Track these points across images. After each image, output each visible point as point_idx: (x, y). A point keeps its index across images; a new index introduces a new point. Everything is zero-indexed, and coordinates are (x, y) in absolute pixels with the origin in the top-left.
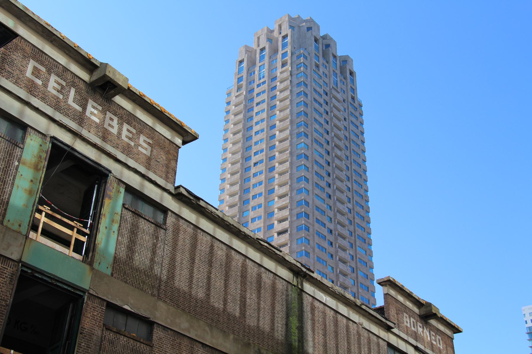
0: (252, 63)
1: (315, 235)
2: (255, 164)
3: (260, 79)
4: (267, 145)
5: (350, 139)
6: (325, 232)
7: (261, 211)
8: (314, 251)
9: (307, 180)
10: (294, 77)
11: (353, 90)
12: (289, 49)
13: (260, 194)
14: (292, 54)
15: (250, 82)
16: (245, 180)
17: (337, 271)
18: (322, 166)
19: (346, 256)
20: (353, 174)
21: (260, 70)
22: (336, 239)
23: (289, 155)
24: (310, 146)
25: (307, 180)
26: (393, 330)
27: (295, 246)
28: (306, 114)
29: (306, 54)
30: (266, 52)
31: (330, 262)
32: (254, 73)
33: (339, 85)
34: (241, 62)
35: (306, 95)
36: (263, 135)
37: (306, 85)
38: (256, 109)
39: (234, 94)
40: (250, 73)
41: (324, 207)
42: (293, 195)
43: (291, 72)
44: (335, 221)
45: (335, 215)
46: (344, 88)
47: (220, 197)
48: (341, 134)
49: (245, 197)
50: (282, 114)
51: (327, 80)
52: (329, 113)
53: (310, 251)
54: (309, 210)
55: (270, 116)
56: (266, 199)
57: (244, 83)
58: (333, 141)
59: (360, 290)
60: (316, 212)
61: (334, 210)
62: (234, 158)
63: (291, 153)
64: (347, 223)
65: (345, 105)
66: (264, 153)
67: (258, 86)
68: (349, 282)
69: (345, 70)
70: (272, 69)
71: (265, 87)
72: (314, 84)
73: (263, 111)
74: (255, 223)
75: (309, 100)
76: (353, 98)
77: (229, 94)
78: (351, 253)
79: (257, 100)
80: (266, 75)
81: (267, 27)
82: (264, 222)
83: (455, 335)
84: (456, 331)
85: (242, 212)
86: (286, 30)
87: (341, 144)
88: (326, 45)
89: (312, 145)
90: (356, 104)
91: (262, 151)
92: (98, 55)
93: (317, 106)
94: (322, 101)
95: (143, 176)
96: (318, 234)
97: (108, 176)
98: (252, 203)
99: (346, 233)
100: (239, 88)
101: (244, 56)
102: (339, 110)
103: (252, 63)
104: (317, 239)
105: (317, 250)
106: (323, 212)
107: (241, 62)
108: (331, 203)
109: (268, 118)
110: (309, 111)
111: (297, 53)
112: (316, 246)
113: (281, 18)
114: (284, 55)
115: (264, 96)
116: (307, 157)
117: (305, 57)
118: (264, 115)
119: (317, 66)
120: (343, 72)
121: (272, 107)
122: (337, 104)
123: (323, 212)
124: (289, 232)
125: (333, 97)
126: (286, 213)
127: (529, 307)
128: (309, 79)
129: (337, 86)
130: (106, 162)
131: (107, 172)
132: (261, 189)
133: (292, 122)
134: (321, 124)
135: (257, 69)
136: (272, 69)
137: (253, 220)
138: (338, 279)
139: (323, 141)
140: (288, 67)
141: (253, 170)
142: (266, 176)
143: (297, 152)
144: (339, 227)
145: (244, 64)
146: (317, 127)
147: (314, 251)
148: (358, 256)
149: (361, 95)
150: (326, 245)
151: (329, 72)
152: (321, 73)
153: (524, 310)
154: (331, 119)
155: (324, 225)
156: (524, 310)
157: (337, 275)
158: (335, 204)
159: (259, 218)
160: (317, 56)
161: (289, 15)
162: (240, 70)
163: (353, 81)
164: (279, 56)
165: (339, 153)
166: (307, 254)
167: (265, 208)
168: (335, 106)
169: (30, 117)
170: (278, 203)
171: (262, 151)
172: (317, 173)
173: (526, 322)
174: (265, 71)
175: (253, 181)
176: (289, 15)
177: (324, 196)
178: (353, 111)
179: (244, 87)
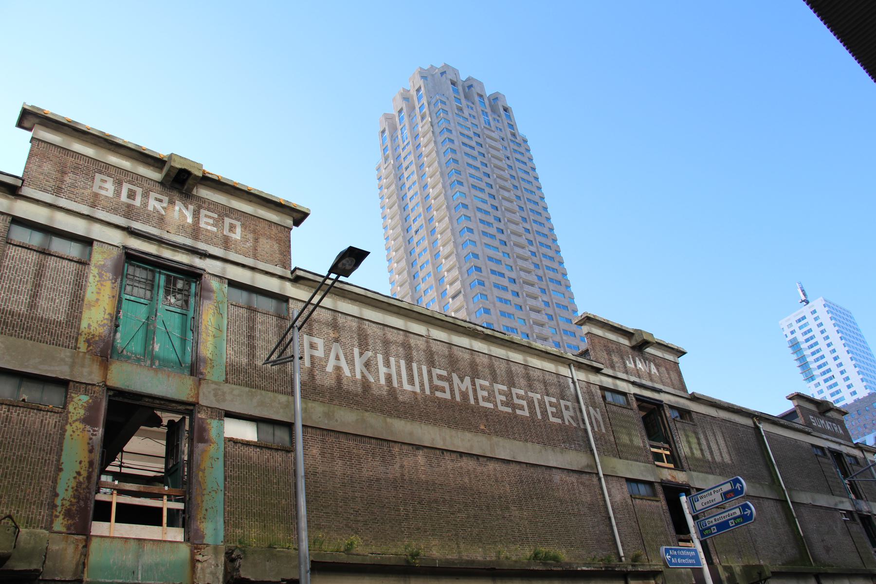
0: (393, 129)
1: (493, 288)
2: (416, 232)
3: (404, 142)
4: (423, 207)
6: (505, 282)
7: (431, 280)
8: (495, 306)
9: (471, 230)
10: (436, 126)
11: (511, 126)
12: (424, 101)
13: (427, 262)
14: (429, 104)
18: (487, 213)
19: (539, 304)
20: (530, 213)
21: (402, 133)
22: (522, 288)
24: (467, 193)
25: (471, 230)
26: (603, 371)
27: (471, 306)
28: (456, 161)
29: (444, 99)
31: (518, 313)
33: (492, 123)
34: (383, 132)
35: (452, 141)
37: (450, 131)
38: (406, 175)
41: (499, 255)
43: (431, 122)
45: (515, 262)
46: (500, 125)
47: (390, 279)
48: (506, 174)
49: (414, 271)
50: (431, 169)
51: (475, 122)
53: (490, 307)
54: (479, 263)
55: (422, 176)
56: (433, 265)
57: (389, 152)
58: (496, 183)
59: (564, 338)
60: (490, 263)
64: (532, 267)
65: (505, 143)
66: (422, 217)
67: (403, 149)
68: (547, 331)
69: (497, 108)
70: (413, 127)
71: (410, 147)
72: (459, 128)
73: (413, 173)
75: (456, 145)
76: (514, 135)
77: (378, 169)
78: (546, 300)
82: (437, 291)
83: (682, 361)
84: (679, 354)
85: (414, 288)
87: (508, 185)
90: (519, 140)
91: (420, 215)
92: (161, 150)
93: (468, 150)
94: (473, 144)
95: (253, 269)
96: (497, 286)
97: (202, 275)
98: (421, 275)
99: (532, 278)
100: (386, 159)
102: (498, 150)
103: (393, 129)
104: (497, 292)
105: (498, 304)
106: (498, 262)
107: (383, 132)
108: (507, 249)
109: (419, 179)
110: (458, 157)
111: (434, 101)
112: (496, 299)
115: (411, 158)
116: (465, 206)
117: (444, 103)
118: (415, 177)
119: (461, 110)
120: (494, 110)
122: (493, 143)
123: (498, 262)
124: (463, 292)
128: (452, 124)
129: (489, 124)
130: (198, 262)
131: (202, 272)
132: (427, 256)
133: (442, 174)
134: (477, 168)
136: (413, 127)
138: (533, 331)
139: (483, 185)
141: (416, 239)
144: (522, 274)
145: (387, 133)
146: (473, 171)
147: (495, 306)
148: (554, 301)
149: (522, 129)
150: (509, 296)
151: (477, 112)
152: (466, 114)
154: (490, 160)
155: (503, 275)
158: (512, 249)
159: (431, 287)
160: (458, 100)
162: (383, 141)
163: (509, 117)
165: (506, 194)
166: (487, 311)
167: (435, 275)
168: (491, 146)
169: (97, 232)
170: (446, 264)
171: (420, 215)
172: (482, 221)
174: (406, 132)
175: (418, 250)
177: (496, 243)
178: (516, 148)
179: (391, 156)
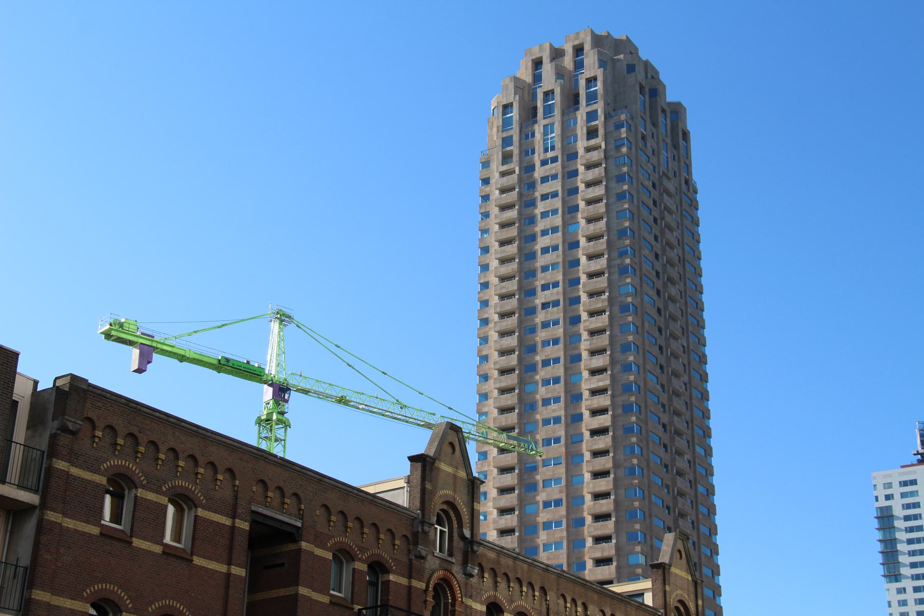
0: (530, 114)
3: (546, 150)
5: (684, 259)
12: (599, 106)
15: (527, 152)
16: (526, 330)
17: (673, 491)
21: (545, 134)
22: (672, 440)
23: (606, 303)
30: (557, 100)
32: (533, 135)
36: (558, 256)
39: (496, 167)
40: (526, 135)
42: (615, 371)
44: (670, 410)
47: (479, 351)
52: (659, 221)
57: (514, 149)
61: (669, 391)
62: (504, 287)
63: (610, 299)
74: (549, 407)
76: (687, 182)
77: (486, 164)
79: (542, 189)
80: (558, 145)
81: (551, 45)
86: (591, 65)
88: (653, 89)
89: (641, 286)
101: (511, 97)
103: (530, 114)
107: (507, 107)
113: (578, 34)
114: (592, 116)
121: (572, 210)
125: (664, 191)
126: (604, 401)
127: (883, 473)
135: (538, 129)
137: (546, 402)
140: (599, 140)
142: (565, 330)
143: (620, 299)
145: (515, 114)
153: (875, 478)
156: (875, 478)
157: (674, 498)
159: (557, 400)
161: (592, 31)
162: (506, 123)
164: (581, 115)
173: (877, 498)
176: (592, 31)
